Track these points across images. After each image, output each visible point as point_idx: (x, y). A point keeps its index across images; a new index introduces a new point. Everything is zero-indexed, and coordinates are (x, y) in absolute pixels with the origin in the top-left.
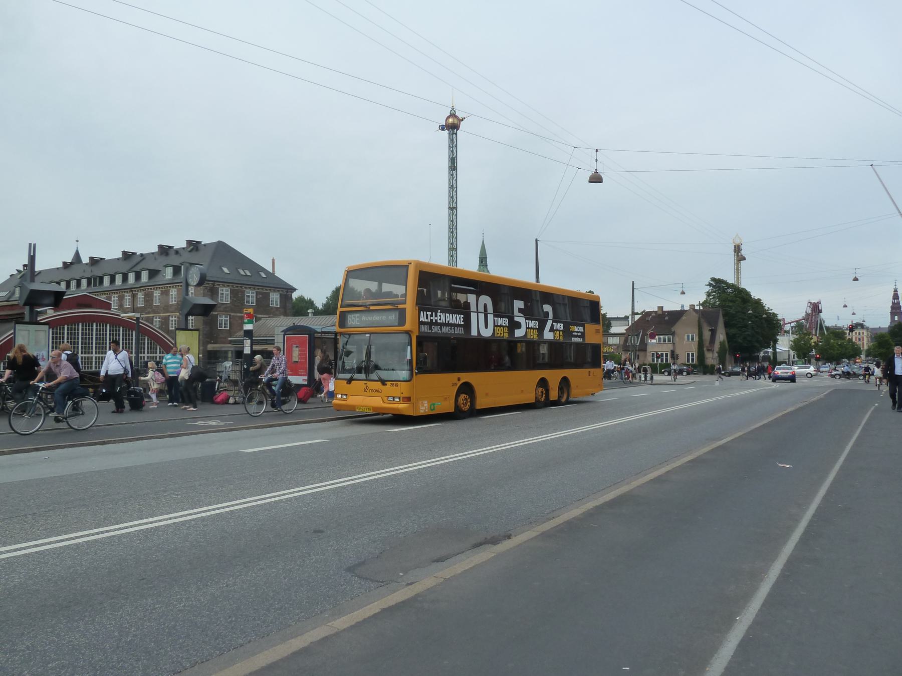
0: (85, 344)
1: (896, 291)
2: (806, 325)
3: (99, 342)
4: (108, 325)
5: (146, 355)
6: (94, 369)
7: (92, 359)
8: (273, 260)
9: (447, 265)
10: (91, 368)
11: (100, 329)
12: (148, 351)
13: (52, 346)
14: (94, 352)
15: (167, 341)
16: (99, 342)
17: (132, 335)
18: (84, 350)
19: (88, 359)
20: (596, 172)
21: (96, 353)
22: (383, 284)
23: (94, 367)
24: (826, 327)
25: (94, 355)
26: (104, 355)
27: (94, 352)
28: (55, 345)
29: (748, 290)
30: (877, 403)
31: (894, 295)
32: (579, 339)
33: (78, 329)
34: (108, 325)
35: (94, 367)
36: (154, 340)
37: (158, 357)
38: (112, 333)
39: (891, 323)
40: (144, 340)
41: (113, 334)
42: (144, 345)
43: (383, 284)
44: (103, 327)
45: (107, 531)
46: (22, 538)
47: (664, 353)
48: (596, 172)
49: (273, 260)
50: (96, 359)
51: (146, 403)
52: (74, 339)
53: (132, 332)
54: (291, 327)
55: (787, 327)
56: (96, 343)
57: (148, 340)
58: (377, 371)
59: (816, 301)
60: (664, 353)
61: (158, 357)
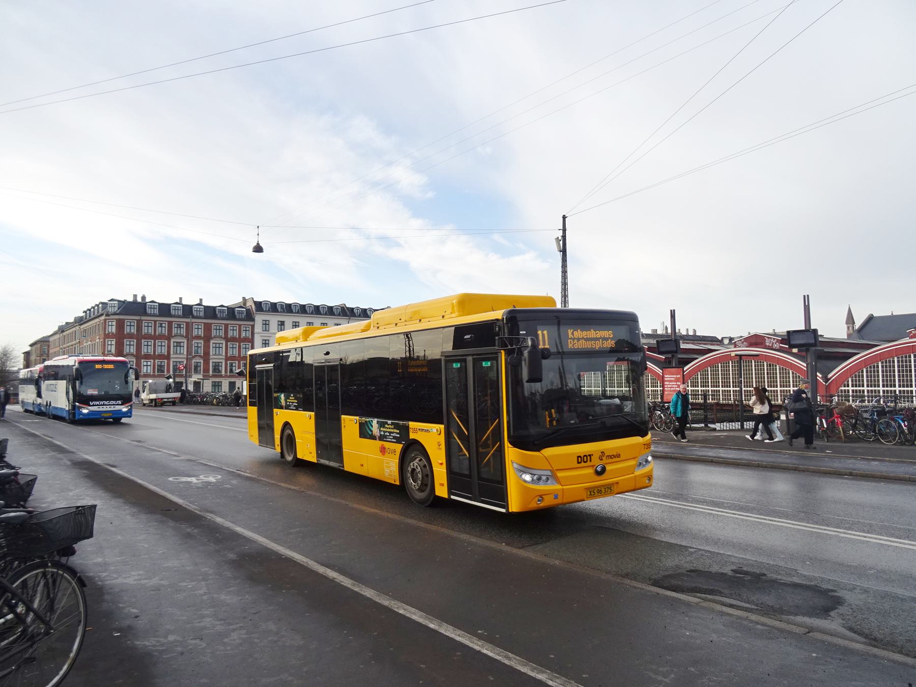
1: (850, 311)
3: (747, 373)
4: (753, 362)
5: (865, 388)
8: (806, 299)
10: (778, 401)
14: (791, 386)
16: (747, 373)
20: (258, 244)
21: (868, 386)
24: (23, 408)
27: (791, 386)
28: (892, 374)
29: (42, 337)
38: (733, 364)
42: (776, 378)
46: (852, 609)
47: (248, 431)
48: (258, 244)
49: (806, 299)
50: (730, 386)
54: (24, 357)
60: (248, 431)
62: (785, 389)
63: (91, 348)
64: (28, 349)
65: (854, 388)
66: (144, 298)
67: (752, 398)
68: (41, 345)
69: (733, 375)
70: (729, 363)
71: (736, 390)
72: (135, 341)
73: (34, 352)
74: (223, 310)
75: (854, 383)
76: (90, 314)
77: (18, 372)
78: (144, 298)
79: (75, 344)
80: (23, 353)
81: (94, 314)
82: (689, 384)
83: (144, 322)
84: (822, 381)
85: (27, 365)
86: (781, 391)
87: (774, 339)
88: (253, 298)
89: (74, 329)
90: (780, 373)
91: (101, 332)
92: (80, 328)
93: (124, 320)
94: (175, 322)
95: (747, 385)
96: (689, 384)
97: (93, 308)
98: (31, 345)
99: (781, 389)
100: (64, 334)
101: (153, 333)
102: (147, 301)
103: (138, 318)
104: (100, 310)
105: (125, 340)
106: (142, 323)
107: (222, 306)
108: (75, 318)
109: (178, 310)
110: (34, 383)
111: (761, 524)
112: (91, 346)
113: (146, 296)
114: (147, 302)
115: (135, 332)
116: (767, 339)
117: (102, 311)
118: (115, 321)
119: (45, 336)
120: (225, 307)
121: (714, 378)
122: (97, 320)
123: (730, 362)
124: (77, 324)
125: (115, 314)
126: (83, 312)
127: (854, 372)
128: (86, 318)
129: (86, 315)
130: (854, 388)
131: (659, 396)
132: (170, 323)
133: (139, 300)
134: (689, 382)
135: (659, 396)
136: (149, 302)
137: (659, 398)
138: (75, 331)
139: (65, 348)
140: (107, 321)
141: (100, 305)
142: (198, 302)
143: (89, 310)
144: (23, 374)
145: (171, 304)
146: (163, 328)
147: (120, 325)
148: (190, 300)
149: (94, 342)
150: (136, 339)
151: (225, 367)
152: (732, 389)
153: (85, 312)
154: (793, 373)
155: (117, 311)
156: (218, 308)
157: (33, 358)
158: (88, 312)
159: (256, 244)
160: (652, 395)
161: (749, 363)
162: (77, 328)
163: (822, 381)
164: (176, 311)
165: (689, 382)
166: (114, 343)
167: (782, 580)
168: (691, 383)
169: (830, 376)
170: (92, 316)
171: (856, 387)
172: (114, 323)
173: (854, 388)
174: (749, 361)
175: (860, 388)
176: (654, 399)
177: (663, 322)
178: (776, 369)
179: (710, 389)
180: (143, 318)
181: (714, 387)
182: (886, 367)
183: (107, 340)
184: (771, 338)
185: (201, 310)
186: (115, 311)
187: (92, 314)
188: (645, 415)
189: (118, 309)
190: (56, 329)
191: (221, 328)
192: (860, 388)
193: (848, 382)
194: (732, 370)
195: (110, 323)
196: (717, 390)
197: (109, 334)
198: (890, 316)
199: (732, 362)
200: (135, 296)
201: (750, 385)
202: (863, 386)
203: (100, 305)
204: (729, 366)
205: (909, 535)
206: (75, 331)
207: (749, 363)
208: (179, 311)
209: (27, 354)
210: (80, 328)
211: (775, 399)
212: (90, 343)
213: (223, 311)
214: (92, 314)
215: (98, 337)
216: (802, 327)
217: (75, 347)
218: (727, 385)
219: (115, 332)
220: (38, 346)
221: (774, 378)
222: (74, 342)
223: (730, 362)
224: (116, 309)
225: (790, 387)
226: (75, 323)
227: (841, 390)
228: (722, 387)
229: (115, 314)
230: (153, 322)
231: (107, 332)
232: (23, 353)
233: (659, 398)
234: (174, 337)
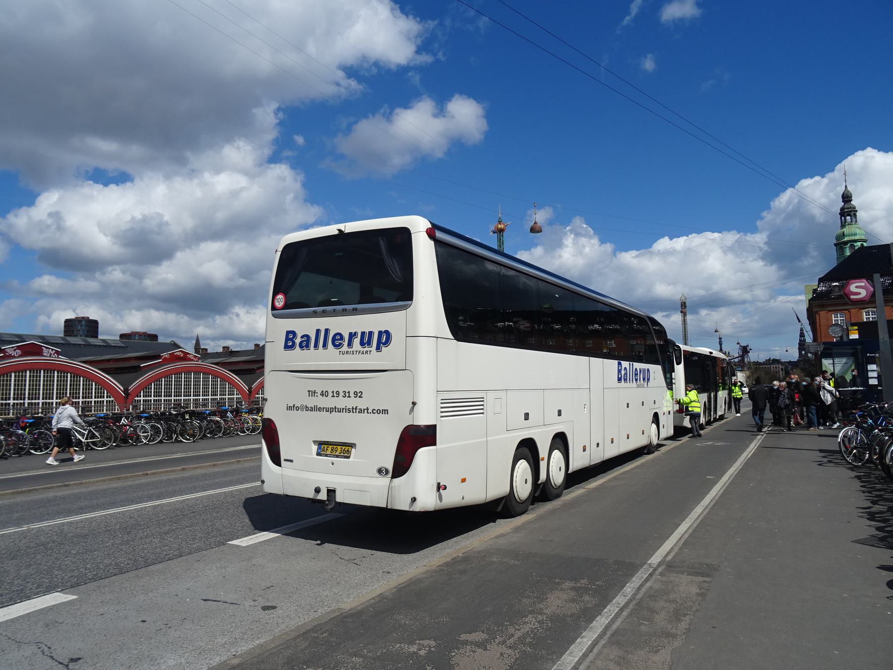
0: (33, 386)
7: (144, 396)
9: (634, 363)
11: (47, 376)
15: (116, 387)
18: (16, 392)
19: (167, 395)
21: (95, 398)
23: (105, 410)
27: (93, 397)
31: (801, 333)
32: (871, 374)
33: (54, 376)
35: (105, 410)
36: (233, 385)
37: (152, 400)
39: (799, 357)
40: (92, 385)
41: (61, 380)
42: (172, 389)
44: (37, 373)
52: (33, 380)
53: (80, 378)
55: (437, 57)
57: (96, 385)
59: (745, 345)
61: (152, 400)
62: (87, 400)
66: (331, 492)
67: (67, 406)
69: (162, 388)
87: (53, 350)
99: (144, 398)
116: (44, 349)
121: (177, 388)
127: (146, 386)
151: (590, 291)
159: (844, 473)
167: (210, 466)
176: (97, 412)
181: (148, 400)
182: (19, 381)
184: (49, 348)
198: (858, 332)
200: (318, 490)
201: (159, 395)
218: (179, 395)
221: (76, 390)
227: (135, 400)
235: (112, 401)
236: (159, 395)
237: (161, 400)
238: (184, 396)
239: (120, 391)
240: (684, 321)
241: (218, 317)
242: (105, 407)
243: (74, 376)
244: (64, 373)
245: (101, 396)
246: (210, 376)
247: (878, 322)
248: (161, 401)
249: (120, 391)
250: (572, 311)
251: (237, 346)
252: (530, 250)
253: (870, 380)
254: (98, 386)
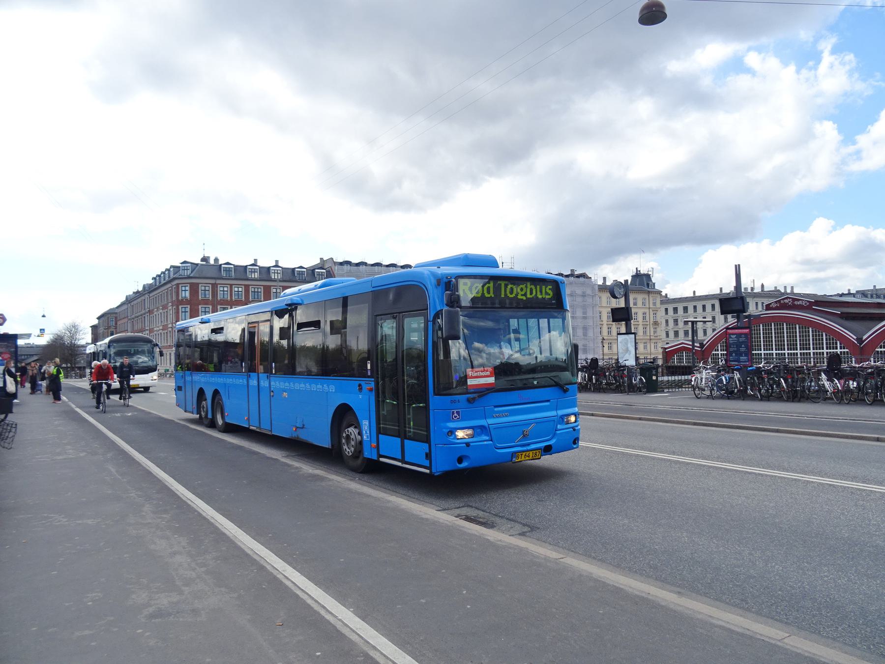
2: (393, 333)
4: (761, 325)
6: (799, 364)
10: (798, 363)
12: (764, 349)
13: (837, 344)
14: (786, 349)
17: (809, 331)
21: (814, 349)
22: (510, 320)
23: (799, 363)
25: (812, 351)
26: (345, 330)
27: (786, 349)
30: (499, 577)
34: (761, 325)
35: (799, 363)
40: (822, 336)
43: (510, 320)
45: (746, 469)
51: (554, 356)
53: (808, 328)
56: (772, 342)
58: (507, 344)
63: (163, 318)
64: (96, 322)
65: (815, 351)
66: (216, 260)
68: (108, 318)
70: (760, 327)
71: (724, 354)
72: (211, 307)
73: (101, 325)
74: (302, 271)
75: (815, 342)
76: (160, 279)
77: (84, 346)
78: (216, 260)
79: (144, 314)
80: (91, 327)
81: (164, 280)
82: (719, 348)
83: (219, 286)
84: (856, 342)
85: (95, 340)
86: (810, 349)
88: (332, 259)
89: (143, 298)
90: (800, 340)
91: (174, 298)
92: (149, 295)
93: (198, 284)
94: (251, 285)
95: (767, 348)
96: (719, 348)
97: (163, 273)
98: (99, 318)
100: (132, 304)
101: (229, 298)
102: (220, 263)
103: (213, 281)
104: (172, 274)
105: (200, 307)
106: (217, 287)
107: (301, 267)
108: (144, 285)
109: (187, 270)
110: (629, 322)
111: (654, 459)
112: (163, 314)
113: (219, 258)
114: (221, 265)
115: (210, 298)
117: (174, 275)
118: (188, 285)
119: (112, 308)
120: (305, 268)
122: (169, 285)
123: (773, 324)
124: (146, 292)
125: (189, 277)
126: (153, 279)
128: (156, 285)
129: (155, 282)
130: (777, 352)
131: (825, 359)
132: (247, 287)
133: (212, 262)
134: (719, 346)
135: (825, 359)
136: (224, 264)
137: (825, 362)
138: (144, 300)
139: (133, 319)
140: (180, 286)
141: (172, 269)
142: (274, 264)
143: (159, 276)
144: (90, 349)
145: (246, 266)
146: (279, 274)
147: (194, 289)
148: (265, 262)
149: (167, 310)
150: (211, 305)
152: (720, 352)
153: (154, 279)
154: (826, 335)
155: (190, 274)
156: (297, 269)
157: (101, 330)
158: (158, 278)
160: (814, 359)
161: (780, 326)
162: (147, 296)
163: (856, 342)
164: (276, 274)
165: (719, 346)
166: (188, 310)
168: (721, 347)
169: (864, 338)
170: (163, 282)
171: (817, 349)
172: (188, 288)
173: (815, 351)
174: (766, 324)
175: (820, 351)
176: (821, 364)
177: (754, 280)
178: (809, 331)
179: (763, 352)
180: (218, 282)
183: (180, 307)
184: (803, 300)
185: (279, 272)
186: (188, 274)
187: (162, 279)
188: (863, 388)
189: (192, 272)
190: (124, 299)
191: (259, 290)
192: (820, 351)
193: (718, 347)
194: (760, 330)
195: (183, 289)
196: (758, 354)
197: (182, 300)
199: (775, 324)
201: (758, 349)
202: (823, 349)
203: (172, 269)
204: (760, 329)
205: (880, 483)
206: (144, 300)
207: (780, 326)
208: (256, 273)
209: (94, 328)
210: (149, 295)
211: (820, 362)
212: (161, 311)
213: (302, 273)
214: (162, 279)
215: (170, 304)
216: (520, 320)
217: (144, 317)
219: (189, 298)
220: (106, 318)
222: (143, 312)
223: (773, 324)
224: (189, 272)
225: (784, 350)
226: (144, 292)
227: (714, 354)
228: (721, 351)
229: (189, 277)
230: (229, 286)
231: (180, 298)
232: (91, 327)
233: (825, 362)
234: (251, 302)
235: (847, 352)
236: (794, 348)
237: (773, 354)
238: (721, 351)
239: (854, 341)
240: (192, 378)
241: (151, 365)
242: (799, 359)
243: (802, 327)
244: (792, 325)
245: (820, 348)
246: (810, 329)
247: (581, 431)
248: (773, 355)
249: (854, 341)
250: (344, 262)
251: (807, 282)
252: (210, 339)
253: (546, 320)
254: (829, 336)
